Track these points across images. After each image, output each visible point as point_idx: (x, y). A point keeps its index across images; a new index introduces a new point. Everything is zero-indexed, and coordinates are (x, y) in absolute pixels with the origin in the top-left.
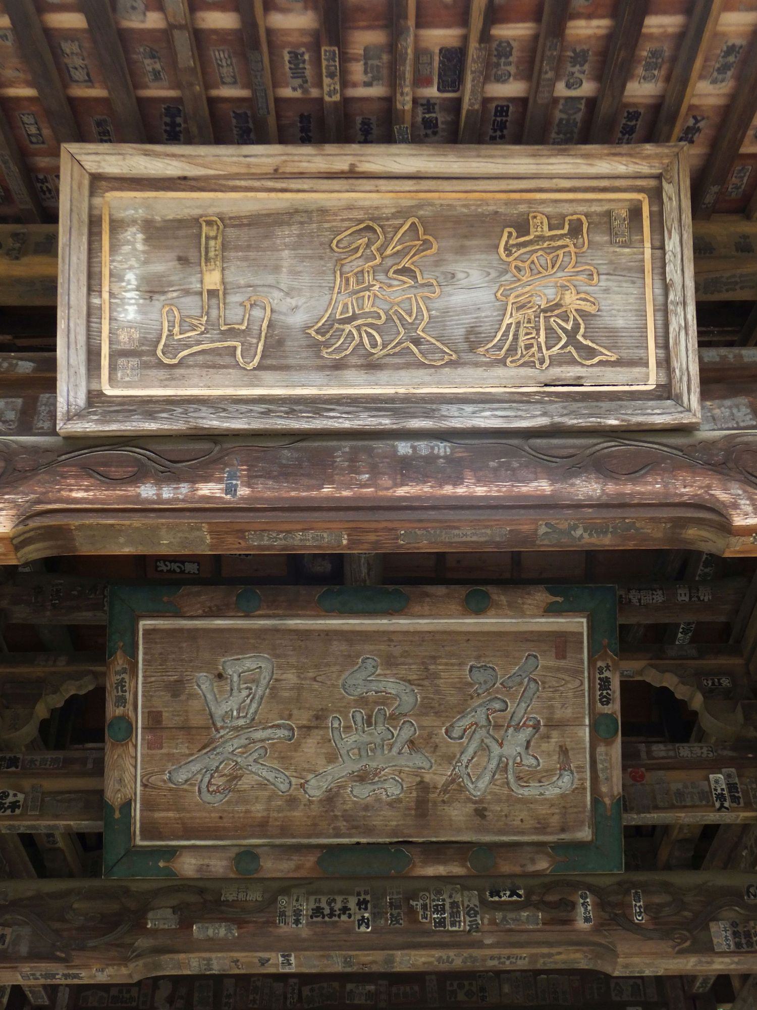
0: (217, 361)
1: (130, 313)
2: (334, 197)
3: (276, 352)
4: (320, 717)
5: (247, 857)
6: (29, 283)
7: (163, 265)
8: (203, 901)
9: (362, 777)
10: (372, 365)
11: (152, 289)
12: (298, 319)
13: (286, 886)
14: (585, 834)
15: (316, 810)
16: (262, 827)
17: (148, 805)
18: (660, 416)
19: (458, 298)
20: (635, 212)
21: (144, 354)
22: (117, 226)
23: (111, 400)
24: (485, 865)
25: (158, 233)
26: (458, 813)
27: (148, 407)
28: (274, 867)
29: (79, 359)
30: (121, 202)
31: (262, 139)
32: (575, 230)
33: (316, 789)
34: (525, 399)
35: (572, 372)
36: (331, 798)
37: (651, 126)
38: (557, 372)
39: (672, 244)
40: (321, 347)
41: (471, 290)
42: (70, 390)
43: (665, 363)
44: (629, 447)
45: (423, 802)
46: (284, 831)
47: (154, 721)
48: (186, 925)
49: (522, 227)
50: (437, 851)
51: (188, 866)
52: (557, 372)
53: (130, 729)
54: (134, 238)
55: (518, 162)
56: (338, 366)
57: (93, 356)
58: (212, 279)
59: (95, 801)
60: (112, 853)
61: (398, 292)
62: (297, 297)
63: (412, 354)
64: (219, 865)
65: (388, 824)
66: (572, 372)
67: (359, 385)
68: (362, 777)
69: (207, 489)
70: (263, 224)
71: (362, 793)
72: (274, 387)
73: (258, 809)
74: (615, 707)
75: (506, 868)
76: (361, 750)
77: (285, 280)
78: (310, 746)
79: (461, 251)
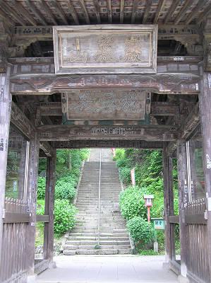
0: (80, 62)
1: (65, 54)
2: (98, 33)
3: (88, 60)
4: (98, 99)
5: (86, 122)
6: (50, 38)
7: (70, 46)
8: (79, 129)
9: (106, 109)
10: (104, 62)
11: (69, 50)
12: (92, 55)
13: (93, 127)
14: (144, 119)
15: (98, 114)
16: (89, 117)
17: (70, 113)
18: (150, 71)
19: (118, 51)
20: (149, 36)
21: (67, 61)
22: (62, 39)
23: (64, 68)
24: (126, 123)
25: (69, 40)
26: (122, 115)
27: (69, 70)
28: (90, 123)
29: (58, 62)
30: (63, 35)
31: (86, 24)
32: (139, 39)
33: (98, 110)
34: (129, 68)
35: (136, 64)
36: (100, 112)
37: (151, 21)
38: (134, 64)
39: (154, 42)
40: (96, 59)
41: (121, 50)
42: (57, 69)
43: (152, 62)
44: (144, 78)
45: (116, 113)
46: (93, 118)
47: (70, 99)
48: (77, 133)
49: (130, 39)
50: (118, 121)
51: (76, 123)
52: (134, 64)
53: (66, 101)
54: (65, 41)
55: (129, 27)
56: (99, 62)
57: (60, 61)
58: (78, 48)
59: (60, 111)
60: (64, 120)
61: (109, 50)
62: (92, 51)
63: (111, 60)
64: (82, 123)
65: (110, 117)
66: (136, 64)
67: (102, 65)
68: (106, 109)
69: (79, 84)
70: (87, 38)
71: (106, 111)
72: (88, 66)
73: (88, 114)
74: (150, 98)
75: (130, 124)
76: (106, 104)
77: (90, 48)
78: (97, 104)
79: (119, 43)
